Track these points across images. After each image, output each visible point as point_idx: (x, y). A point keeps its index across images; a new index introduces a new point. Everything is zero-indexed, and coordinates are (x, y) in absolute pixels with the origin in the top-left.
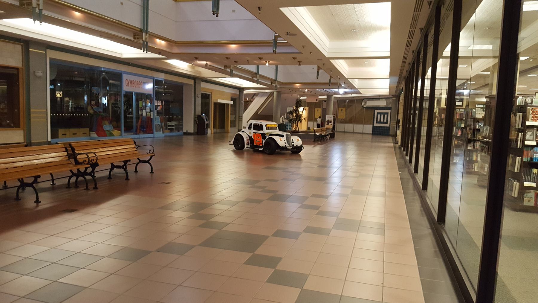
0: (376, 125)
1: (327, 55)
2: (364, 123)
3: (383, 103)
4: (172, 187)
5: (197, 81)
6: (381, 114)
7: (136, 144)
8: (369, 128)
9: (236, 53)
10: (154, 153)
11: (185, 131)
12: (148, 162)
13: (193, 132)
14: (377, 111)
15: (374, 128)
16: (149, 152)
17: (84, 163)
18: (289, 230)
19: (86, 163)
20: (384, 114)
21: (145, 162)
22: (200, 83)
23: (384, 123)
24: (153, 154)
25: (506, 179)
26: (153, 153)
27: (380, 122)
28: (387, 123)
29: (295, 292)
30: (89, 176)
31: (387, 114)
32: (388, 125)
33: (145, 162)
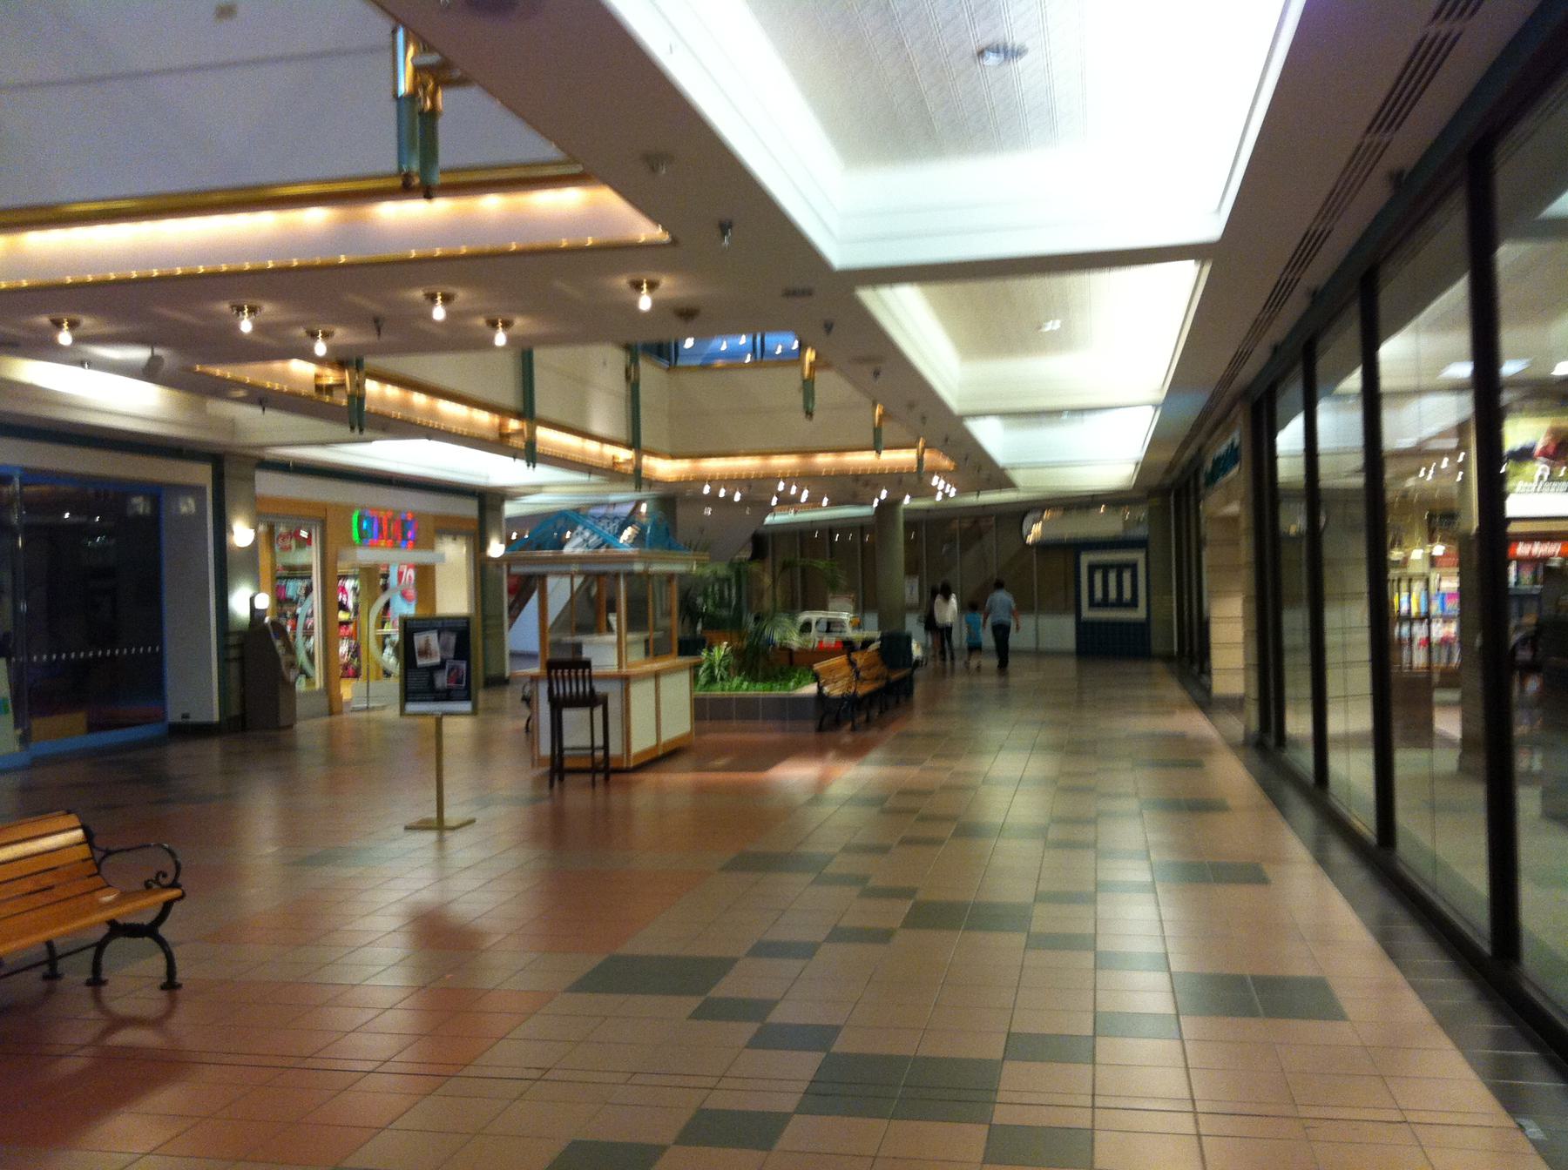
0: (1088, 614)
1: (839, 254)
2: (708, 716)
3: (1105, 524)
4: (419, 988)
5: (228, 469)
6: (1106, 568)
7: (97, 842)
8: (1060, 631)
9: (343, 259)
10: (179, 887)
11: (174, 716)
12: (149, 931)
13: (216, 718)
14: (1086, 559)
15: (1083, 628)
16: (159, 884)
17: (159, 884)
18: (974, 1055)
19: (164, 881)
20: (1120, 568)
21: (134, 931)
22: (252, 479)
23: (1120, 603)
24: (175, 893)
25: (549, 762)
26: (174, 885)
27: (1105, 603)
28: (1133, 604)
29: (970, 1140)
30: (146, 939)
31: (1133, 567)
32: (1140, 614)
33: (134, 931)
